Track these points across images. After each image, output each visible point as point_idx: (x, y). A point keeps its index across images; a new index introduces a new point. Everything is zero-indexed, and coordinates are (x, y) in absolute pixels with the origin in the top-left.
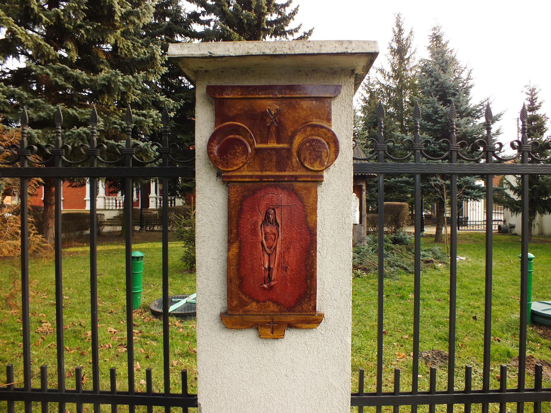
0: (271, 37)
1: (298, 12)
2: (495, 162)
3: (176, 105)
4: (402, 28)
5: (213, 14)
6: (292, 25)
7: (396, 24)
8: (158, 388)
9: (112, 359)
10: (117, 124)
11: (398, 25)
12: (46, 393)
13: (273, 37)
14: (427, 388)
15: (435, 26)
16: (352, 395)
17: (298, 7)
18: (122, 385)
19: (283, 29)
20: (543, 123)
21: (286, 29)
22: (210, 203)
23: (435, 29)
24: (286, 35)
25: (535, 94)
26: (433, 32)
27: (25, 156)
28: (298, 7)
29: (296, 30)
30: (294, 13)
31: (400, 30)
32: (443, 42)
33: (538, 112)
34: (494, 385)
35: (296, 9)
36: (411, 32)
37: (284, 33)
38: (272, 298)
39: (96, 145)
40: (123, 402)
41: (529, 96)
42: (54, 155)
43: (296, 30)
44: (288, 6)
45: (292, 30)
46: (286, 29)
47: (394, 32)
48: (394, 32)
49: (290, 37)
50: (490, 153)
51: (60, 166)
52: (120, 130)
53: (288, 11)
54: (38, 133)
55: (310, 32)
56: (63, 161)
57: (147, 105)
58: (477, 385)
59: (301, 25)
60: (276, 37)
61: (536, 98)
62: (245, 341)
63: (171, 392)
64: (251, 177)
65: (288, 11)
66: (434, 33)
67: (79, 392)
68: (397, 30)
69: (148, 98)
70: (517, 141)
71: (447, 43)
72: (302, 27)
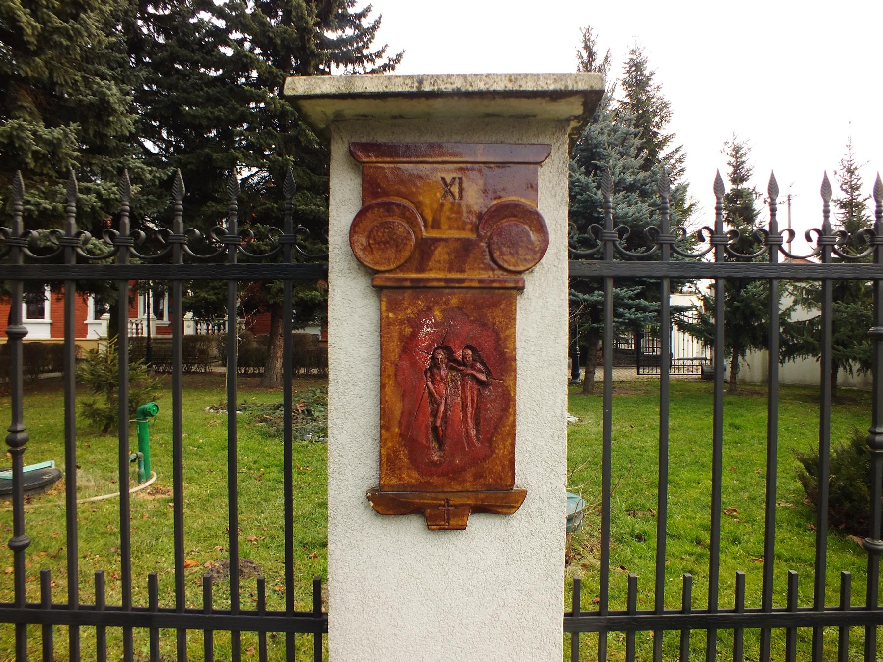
0: (338, 66)
1: (380, 26)
2: (834, 260)
3: (157, 175)
4: (594, 50)
5: (234, 32)
6: (373, 48)
7: (583, 45)
8: (276, 604)
9: (96, 556)
10: (32, 205)
11: (587, 47)
12: (129, 613)
13: (342, 66)
14: (705, 606)
15: (633, 47)
16: (565, 615)
17: (380, 18)
18: (113, 597)
19: (361, 53)
20: (751, 202)
21: (365, 52)
22: (352, 323)
23: (633, 52)
24: (363, 62)
25: (742, 156)
26: (632, 56)
27: (20, 247)
28: (380, 18)
29: (379, 55)
30: (374, 28)
31: (591, 55)
32: (646, 73)
33: (744, 186)
34: (779, 602)
35: (378, 22)
36: (607, 58)
37: (359, 60)
38: (446, 470)
39: (128, 232)
40: (35, 620)
41: (733, 160)
42: (65, 246)
43: (379, 55)
44: (365, 17)
45: (371, 55)
46: (365, 52)
47: (581, 57)
48: (581, 57)
49: (369, 66)
50: (828, 248)
51: (73, 262)
52: (37, 213)
53: (366, 23)
54: (261, 205)
55: (399, 56)
56: (26, 255)
57: (108, 174)
58: (753, 601)
59: (386, 46)
60: (346, 66)
61: (743, 162)
62: (407, 535)
63: (269, 609)
64: (439, 280)
65: (366, 23)
66: (631, 59)
67: (181, 612)
68: (585, 55)
69: (111, 163)
70: (816, 230)
71: (652, 74)
72: (387, 49)
